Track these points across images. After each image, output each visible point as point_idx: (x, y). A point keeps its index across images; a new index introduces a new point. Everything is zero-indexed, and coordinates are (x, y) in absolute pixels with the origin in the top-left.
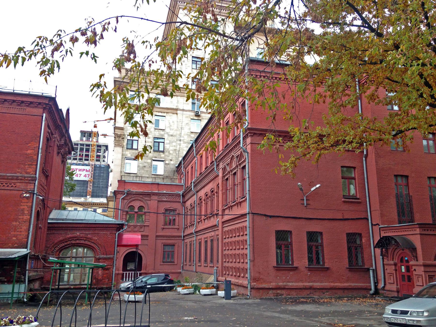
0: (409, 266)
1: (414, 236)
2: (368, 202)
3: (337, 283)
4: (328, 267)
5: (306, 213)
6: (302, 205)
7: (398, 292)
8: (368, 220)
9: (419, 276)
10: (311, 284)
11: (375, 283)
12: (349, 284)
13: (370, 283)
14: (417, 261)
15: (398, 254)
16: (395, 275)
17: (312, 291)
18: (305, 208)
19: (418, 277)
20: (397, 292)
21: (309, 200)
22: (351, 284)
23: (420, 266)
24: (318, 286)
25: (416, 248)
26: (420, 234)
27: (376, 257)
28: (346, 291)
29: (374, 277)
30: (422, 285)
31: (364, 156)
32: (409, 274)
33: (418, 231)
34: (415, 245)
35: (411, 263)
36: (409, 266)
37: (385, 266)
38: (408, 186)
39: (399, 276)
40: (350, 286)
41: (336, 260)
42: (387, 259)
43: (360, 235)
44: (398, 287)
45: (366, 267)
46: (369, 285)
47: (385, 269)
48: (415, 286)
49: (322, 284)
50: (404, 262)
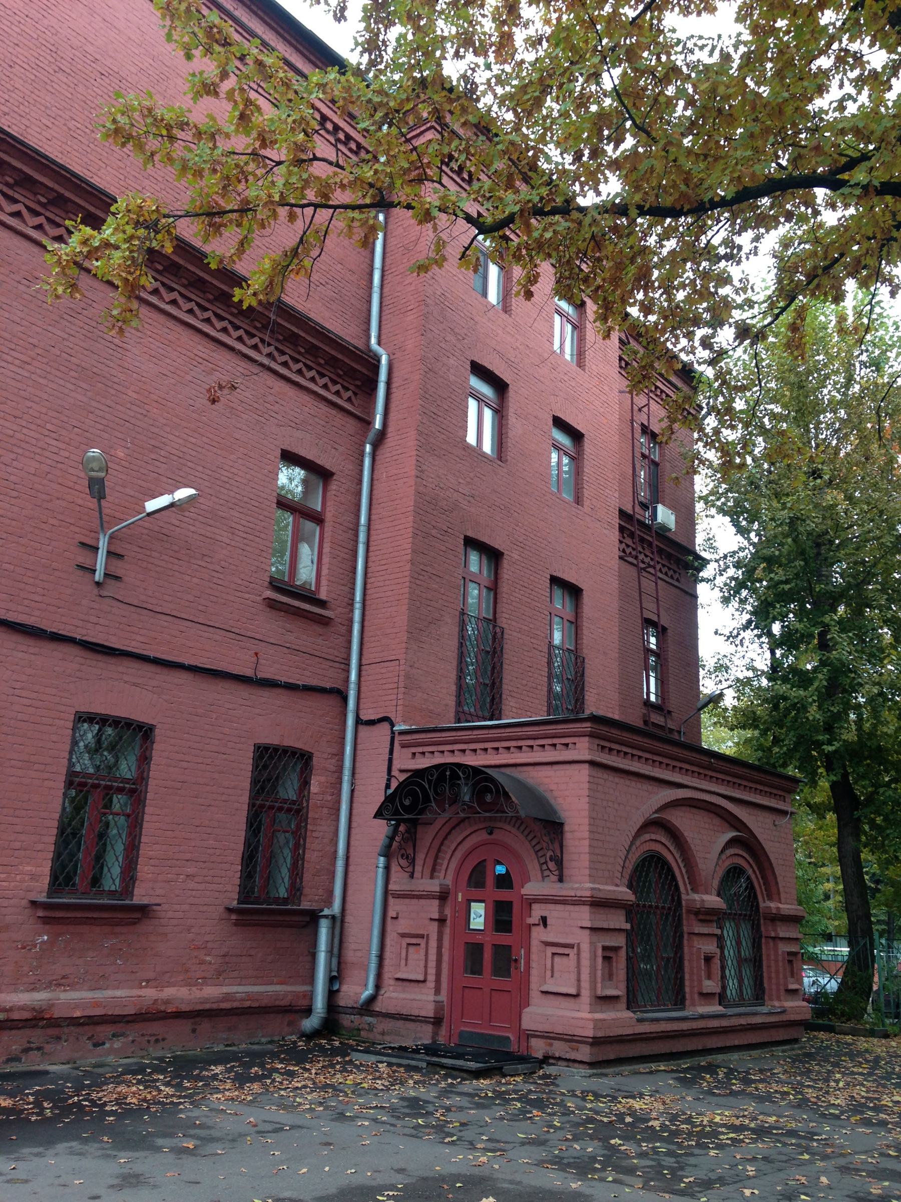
0: (510, 904)
1: (560, 770)
2: (356, 628)
3: (173, 985)
4: (145, 901)
5: (93, 619)
6: (80, 573)
7: (437, 1021)
8: (345, 699)
9: (561, 949)
10: (39, 997)
11: (332, 980)
12: (225, 989)
13: (311, 979)
14: (561, 880)
15: (459, 855)
16: (433, 944)
17: (37, 1036)
18: (96, 591)
19: (554, 954)
20: (433, 1024)
21: (120, 556)
22: (235, 989)
23: (577, 902)
24: (77, 1006)
25: (562, 825)
26: (592, 763)
27: (351, 860)
28: (205, 1026)
29: (330, 952)
30: (573, 991)
31: (371, 435)
32: (504, 939)
33: (583, 749)
34: (557, 807)
35: (532, 888)
36: (510, 904)
37: (391, 901)
38: (496, 594)
39: (452, 948)
40: (227, 997)
41: (190, 871)
42: (410, 869)
43: (304, 758)
44: (439, 998)
45: (305, 905)
46: (307, 988)
47: (391, 913)
48: (535, 995)
49: (98, 995)
50: (490, 882)
